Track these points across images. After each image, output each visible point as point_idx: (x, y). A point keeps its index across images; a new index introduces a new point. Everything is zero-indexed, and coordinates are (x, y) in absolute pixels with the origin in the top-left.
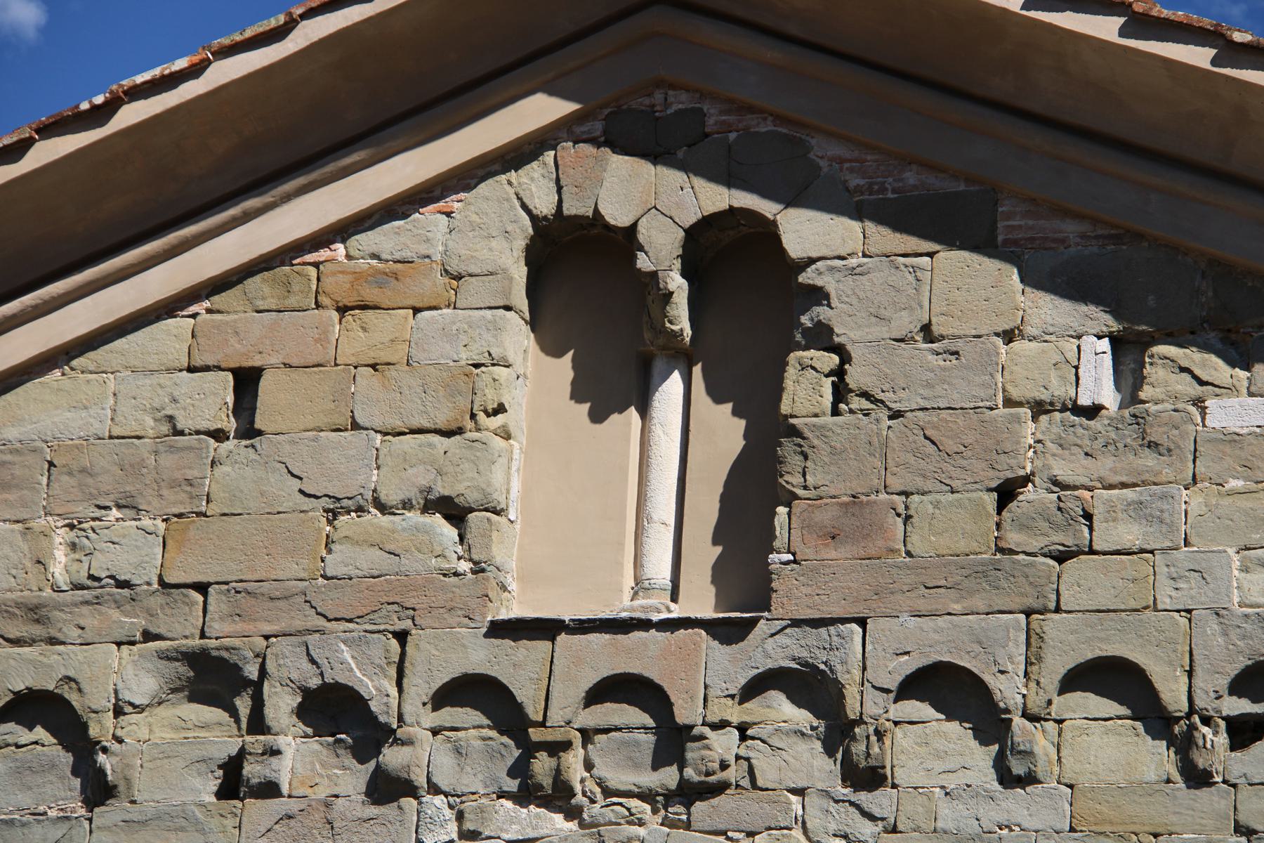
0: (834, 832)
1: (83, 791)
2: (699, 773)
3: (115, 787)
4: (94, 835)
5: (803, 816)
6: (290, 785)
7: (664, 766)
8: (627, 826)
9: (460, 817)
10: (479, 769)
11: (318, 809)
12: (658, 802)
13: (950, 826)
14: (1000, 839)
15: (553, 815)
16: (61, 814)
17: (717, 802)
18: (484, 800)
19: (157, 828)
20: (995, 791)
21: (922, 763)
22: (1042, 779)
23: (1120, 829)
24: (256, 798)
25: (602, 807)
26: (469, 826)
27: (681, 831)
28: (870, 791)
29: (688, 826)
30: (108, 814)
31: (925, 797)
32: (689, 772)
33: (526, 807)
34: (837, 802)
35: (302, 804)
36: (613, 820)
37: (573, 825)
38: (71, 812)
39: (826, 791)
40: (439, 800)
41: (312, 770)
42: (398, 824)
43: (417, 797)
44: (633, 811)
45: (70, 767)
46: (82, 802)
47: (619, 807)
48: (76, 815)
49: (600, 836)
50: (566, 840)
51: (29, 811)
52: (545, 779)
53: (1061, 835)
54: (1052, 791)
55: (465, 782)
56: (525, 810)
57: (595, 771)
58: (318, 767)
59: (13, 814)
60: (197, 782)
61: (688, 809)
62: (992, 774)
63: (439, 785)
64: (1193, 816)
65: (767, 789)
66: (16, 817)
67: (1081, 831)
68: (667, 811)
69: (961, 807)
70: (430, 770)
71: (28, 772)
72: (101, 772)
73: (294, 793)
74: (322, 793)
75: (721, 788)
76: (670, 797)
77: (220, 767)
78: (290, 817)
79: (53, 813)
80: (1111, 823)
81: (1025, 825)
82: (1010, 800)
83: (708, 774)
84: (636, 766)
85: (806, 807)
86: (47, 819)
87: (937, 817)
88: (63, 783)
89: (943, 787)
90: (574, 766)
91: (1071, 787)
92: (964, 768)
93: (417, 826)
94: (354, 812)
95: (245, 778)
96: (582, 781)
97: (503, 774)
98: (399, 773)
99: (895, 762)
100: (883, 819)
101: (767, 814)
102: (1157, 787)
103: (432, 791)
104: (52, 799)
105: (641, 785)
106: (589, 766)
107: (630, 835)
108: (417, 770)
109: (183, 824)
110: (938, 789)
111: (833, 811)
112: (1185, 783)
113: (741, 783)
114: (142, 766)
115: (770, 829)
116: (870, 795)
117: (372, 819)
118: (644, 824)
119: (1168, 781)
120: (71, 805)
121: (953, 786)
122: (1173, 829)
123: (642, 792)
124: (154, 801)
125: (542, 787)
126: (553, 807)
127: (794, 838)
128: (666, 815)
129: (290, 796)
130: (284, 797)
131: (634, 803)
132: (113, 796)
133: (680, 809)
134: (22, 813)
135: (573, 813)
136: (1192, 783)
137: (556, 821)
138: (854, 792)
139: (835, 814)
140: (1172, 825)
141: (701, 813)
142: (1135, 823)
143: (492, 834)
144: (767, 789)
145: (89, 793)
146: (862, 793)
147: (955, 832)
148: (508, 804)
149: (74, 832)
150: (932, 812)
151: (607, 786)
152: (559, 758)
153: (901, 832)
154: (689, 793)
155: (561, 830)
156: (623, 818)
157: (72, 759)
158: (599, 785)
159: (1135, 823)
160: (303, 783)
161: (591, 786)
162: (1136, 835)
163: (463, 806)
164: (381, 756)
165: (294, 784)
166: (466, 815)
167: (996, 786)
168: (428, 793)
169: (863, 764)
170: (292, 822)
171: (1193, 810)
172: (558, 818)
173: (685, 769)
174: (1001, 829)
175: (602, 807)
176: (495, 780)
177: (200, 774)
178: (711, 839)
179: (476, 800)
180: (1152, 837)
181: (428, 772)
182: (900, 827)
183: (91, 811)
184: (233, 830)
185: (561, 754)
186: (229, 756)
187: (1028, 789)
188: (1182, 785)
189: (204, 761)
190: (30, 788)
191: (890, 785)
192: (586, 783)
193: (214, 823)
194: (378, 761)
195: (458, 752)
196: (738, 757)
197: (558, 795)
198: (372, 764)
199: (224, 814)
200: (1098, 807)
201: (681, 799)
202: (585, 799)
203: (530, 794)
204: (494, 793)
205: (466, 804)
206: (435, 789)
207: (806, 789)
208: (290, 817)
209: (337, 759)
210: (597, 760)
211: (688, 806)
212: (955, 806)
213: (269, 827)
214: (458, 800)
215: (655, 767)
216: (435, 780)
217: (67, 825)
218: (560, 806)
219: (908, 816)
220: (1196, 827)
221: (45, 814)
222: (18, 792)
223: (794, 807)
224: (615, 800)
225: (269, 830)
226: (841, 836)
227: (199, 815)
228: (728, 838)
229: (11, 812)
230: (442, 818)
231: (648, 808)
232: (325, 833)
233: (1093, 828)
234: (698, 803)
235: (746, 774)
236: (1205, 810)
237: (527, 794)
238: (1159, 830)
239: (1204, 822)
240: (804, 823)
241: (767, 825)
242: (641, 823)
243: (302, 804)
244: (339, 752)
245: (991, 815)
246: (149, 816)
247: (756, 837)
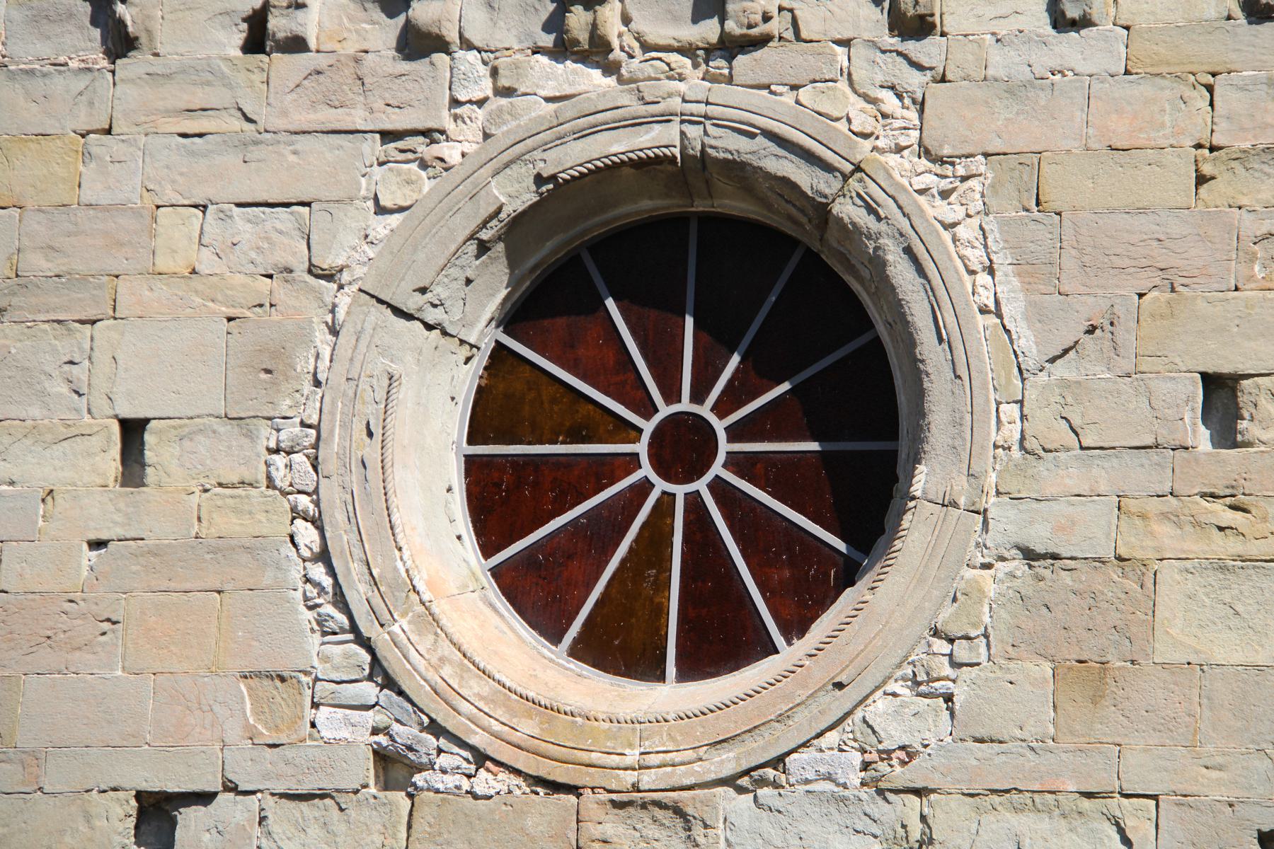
0: (881, 83)
1: (104, 42)
2: (741, 26)
3: (137, 38)
4: (118, 87)
5: (849, 68)
6: (317, 39)
7: (704, 19)
8: (667, 81)
9: (495, 72)
10: (512, 24)
11: (347, 64)
12: (698, 56)
13: (1002, 73)
14: (1053, 84)
15: (590, 70)
16: (83, 65)
17: (760, 55)
18: (518, 56)
19: (182, 82)
20: (1048, 36)
21: (972, 10)
22: (1097, 22)
23: (1176, 69)
24: (283, 53)
25: (641, 62)
26: (504, 82)
27: (723, 85)
28: (918, 40)
29: (730, 80)
30: (130, 66)
31: (975, 45)
32: (731, 25)
33: (563, 63)
34: (884, 52)
35: (331, 59)
36: (653, 75)
37: (611, 81)
38: (93, 64)
39: (873, 41)
40: (472, 56)
41: (340, 25)
42: (431, 80)
43: (449, 53)
44: (673, 66)
45: (89, 16)
46: (104, 53)
47: (659, 62)
48: (98, 67)
49: (639, 91)
50: (604, 96)
51: (49, 61)
52: (581, 33)
53: (1116, 78)
54: (1107, 33)
55: (498, 37)
56: (561, 66)
57: (633, 26)
58: (345, 20)
59: (33, 63)
60: (221, 36)
61: (730, 63)
62: (1045, 19)
63: (472, 40)
64: (1253, 52)
65: (811, 41)
66: (37, 67)
67: (1136, 74)
68: (708, 65)
69: (1012, 53)
70: (462, 24)
71: (45, 21)
72: (121, 23)
73: (322, 48)
74: (351, 48)
75: (763, 41)
76: (711, 51)
77: (244, 20)
78: (319, 73)
79: (74, 64)
80: (1168, 64)
81: (1079, 69)
82: (1064, 44)
83: (750, 26)
84: (676, 19)
85: (852, 58)
86: (69, 70)
87: (988, 64)
88: (82, 33)
89: (993, 34)
90: (610, 20)
91: (1127, 28)
92: (1017, 13)
93: (451, 83)
94: (385, 68)
95: (271, 32)
96: (620, 35)
97: (538, 29)
98: (430, 28)
99: (945, 9)
100: (931, 69)
101: (812, 66)
102: (1217, 24)
103: (464, 46)
104: (72, 50)
105: (681, 39)
106: (626, 20)
107: (670, 90)
108: (448, 25)
109: (209, 78)
110: (989, 36)
111: (880, 61)
112: (1246, 18)
113: (784, 35)
114: (163, 18)
115: (815, 81)
116: (918, 44)
117: (404, 75)
118: (684, 79)
119: (1229, 18)
120: (92, 56)
121: (1004, 32)
122: (1232, 67)
123: (682, 46)
124: (177, 54)
125: (579, 42)
126: (589, 63)
127: (840, 90)
128: (707, 70)
129: (318, 51)
130: (311, 51)
131: (674, 58)
132: (134, 48)
133: (721, 63)
134: (42, 63)
135: (611, 69)
136: (1253, 19)
137: (594, 76)
138: (902, 41)
139: (882, 64)
140: (1232, 62)
141: (743, 67)
142: (1192, 63)
143: (528, 91)
144: (811, 41)
145: (110, 45)
146: (910, 42)
147: (1006, 79)
148: (543, 60)
149: (97, 84)
150: (982, 59)
151: (645, 41)
152: (595, 12)
153: (950, 81)
154: (731, 47)
155: (600, 86)
156: (662, 73)
157: (90, 8)
158: (637, 39)
159: (1192, 63)
160: (330, 38)
161: (629, 40)
162: (1194, 75)
163: (497, 63)
164: (410, 10)
165: (322, 39)
166: (501, 71)
167: (1049, 30)
168: (461, 49)
169: (911, 12)
170: (321, 78)
171: (1254, 46)
172: (596, 74)
173: (726, 22)
174: (1053, 74)
175: (641, 62)
176: (529, 35)
177: (223, 27)
178: (754, 93)
179: (510, 56)
180: (1210, 76)
181: (460, 27)
182: (949, 76)
183: (114, 63)
184: (261, 85)
185: (597, 8)
186: (253, 9)
187: (1083, 32)
188: (1243, 21)
189: (227, 13)
190: (49, 38)
191: (939, 33)
192: (624, 38)
193: (241, 77)
194: (407, 16)
195: (490, 6)
196: (781, 9)
197: (594, 50)
198: (401, 19)
199: (250, 68)
200: (1155, 48)
201: (723, 53)
202: (623, 54)
203: (566, 49)
204: (529, 48)
205: (499, 60)
206: (467, 45)
207: (852, 40)
208: (319, 73)
209: (364, 13)
210: (633, 13)
211: (730, 59)
212: (1007, 53)
213: (297, 82)
214: (492, 56)
215: (696, 20)
216: (467, 35)
217: (89, 76)
218: (597, 62)
219: (958, 64)
220: (1257, 64)
221: (66, 64)
222: (35, 41)
223: (839, 58)
224: (654, 54)
225: (298, 86)
226: (888, 87)
227: (225, 70)
228: (772, 92)
229: (31, 62)
230: (476, 74)
231: (688, 62)
232: (356, 89)
233: (1149, 70)
234: (739, 56)
235: (790, 26)
236: (1266, 45)
237: (563, 49)
238: (1217, 69)
239: (1264, 58)
240: (850, 74)
241: (811, 77)
242: (681, 78)
243: (331, 59)
244: (366, 5)
245: (1043, 60)
246: (174, 69)
247: (801, 90)
